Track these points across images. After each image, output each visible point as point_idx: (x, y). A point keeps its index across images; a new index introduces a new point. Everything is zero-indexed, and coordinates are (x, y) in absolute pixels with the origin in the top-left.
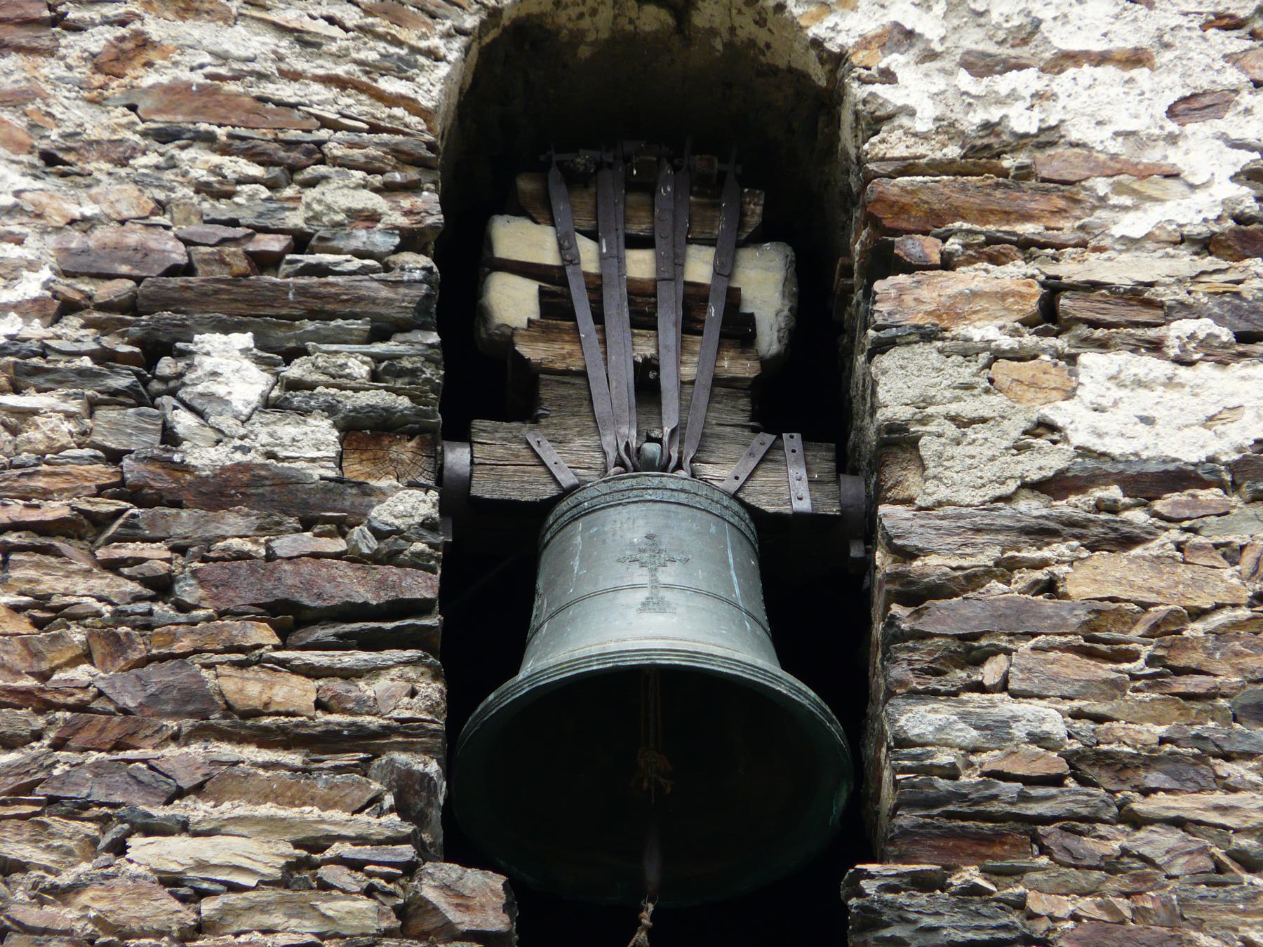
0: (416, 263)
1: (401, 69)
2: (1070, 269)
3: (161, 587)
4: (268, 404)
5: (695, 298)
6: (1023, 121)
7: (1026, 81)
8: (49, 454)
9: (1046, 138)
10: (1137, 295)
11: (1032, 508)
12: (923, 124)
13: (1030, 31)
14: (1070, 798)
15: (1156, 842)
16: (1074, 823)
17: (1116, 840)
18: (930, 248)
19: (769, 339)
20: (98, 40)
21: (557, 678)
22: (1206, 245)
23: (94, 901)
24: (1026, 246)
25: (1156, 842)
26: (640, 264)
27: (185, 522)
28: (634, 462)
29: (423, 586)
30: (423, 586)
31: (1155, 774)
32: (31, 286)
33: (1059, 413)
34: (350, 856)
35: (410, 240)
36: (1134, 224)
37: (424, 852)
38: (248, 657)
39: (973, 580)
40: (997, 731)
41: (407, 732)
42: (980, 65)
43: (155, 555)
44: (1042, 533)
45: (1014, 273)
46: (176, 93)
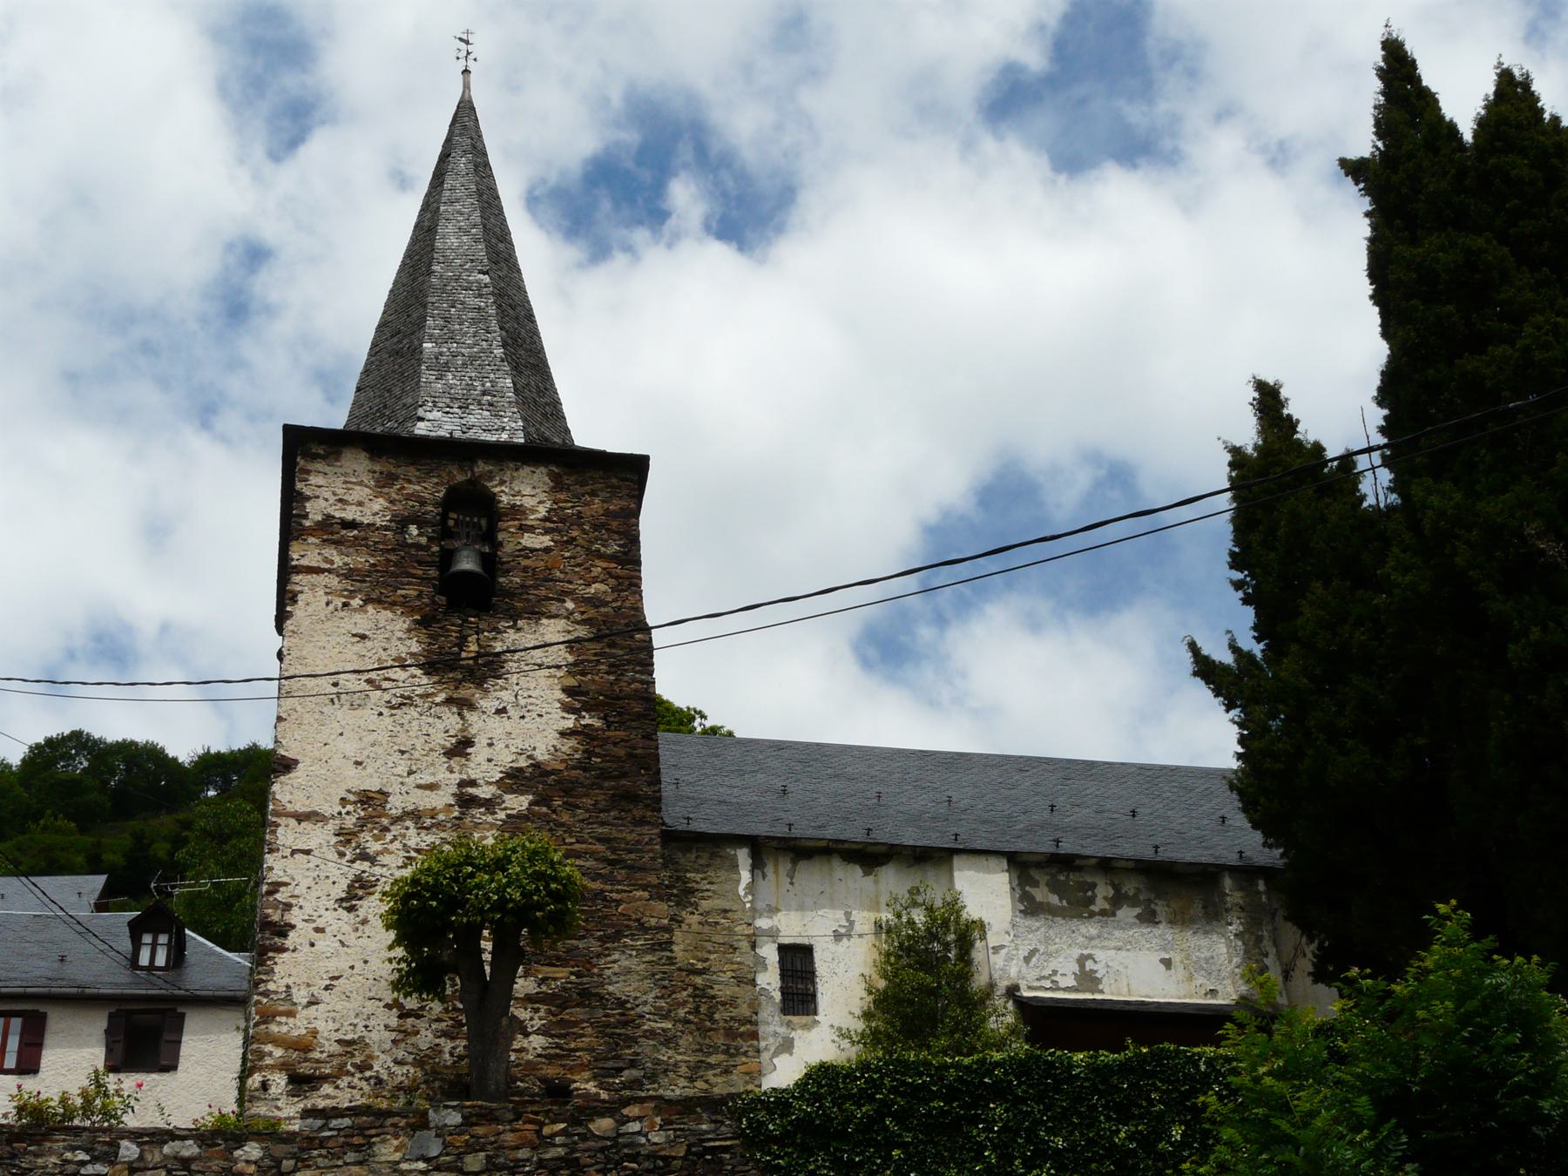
0: (438, 517)
1: (438, 492)
2: (523, 522)
3: (403, 558)
4: (418, 535)
5: (468, 522)
6: (518, 503)
7: (519, 498)
8: (389, 539)
9: (522, 505)
10: (532, 526)
11: (517, 553)
12: (505, 502)
13: (520, 492)
14: (520, 591)
15: (531, 597)
16: (521, 594)
17: (526, 597)
18: (505, 519)
19: (484, 528)
20: (398, 487)
21: (1155, 1000)
22: (541, 520)
23: (393, 598)
24: (518, 519)
25: (531, 597)
26: (468, 519)
27: (406, 549)
28: (466, 544)
29: (437, 559)
30: (437, 559)
31: (1043, 850)
32: (388, 518)
33: (521, 541)
34: (728, 832)
35: (437, 514)
36: (532, 517)
37: (436, 594)
38: (415, 568)
39: (509, 562)
40: (511, 582)
41: (434, 578)
42: (513, 496)
43: (402, 553)
44: (518, 556)
45: (516, 522)
46: (407, 494)
